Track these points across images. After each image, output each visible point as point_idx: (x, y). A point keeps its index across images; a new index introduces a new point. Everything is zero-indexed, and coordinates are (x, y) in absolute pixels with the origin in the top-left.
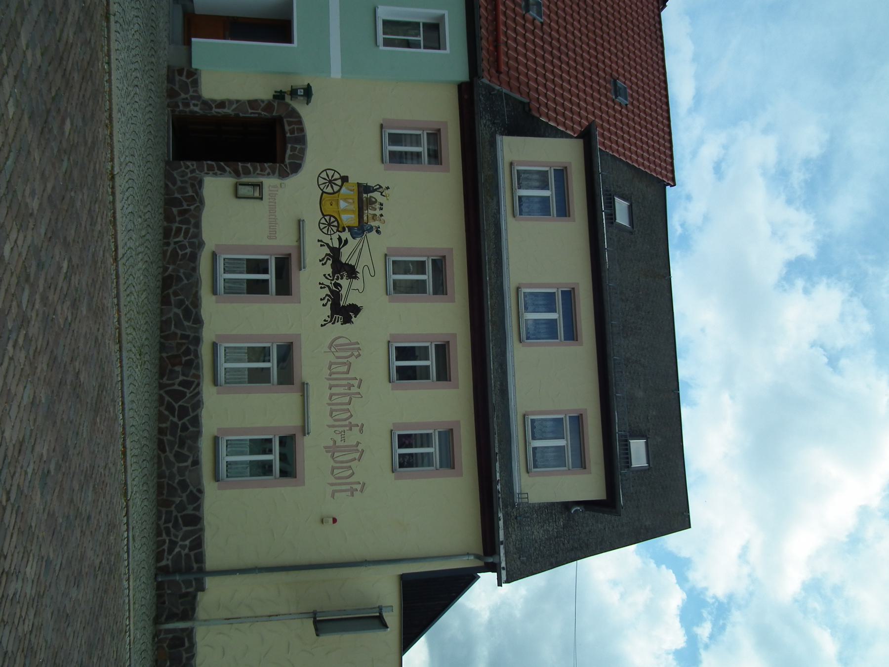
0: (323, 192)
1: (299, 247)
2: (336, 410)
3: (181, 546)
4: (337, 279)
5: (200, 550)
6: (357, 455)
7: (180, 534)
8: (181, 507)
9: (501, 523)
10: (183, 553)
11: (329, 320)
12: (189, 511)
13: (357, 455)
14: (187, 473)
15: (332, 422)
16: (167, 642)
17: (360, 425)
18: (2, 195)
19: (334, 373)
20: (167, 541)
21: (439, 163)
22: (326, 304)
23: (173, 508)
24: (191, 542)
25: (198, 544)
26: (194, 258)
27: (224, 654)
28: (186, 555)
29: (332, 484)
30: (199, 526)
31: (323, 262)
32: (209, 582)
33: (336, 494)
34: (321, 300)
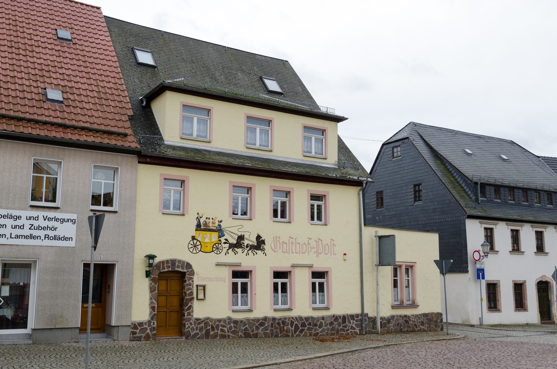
0: (201, 251)
1: (229, 265)
2: (302, 251)
3: (353, 324)
4: (244, 246)
8: (339, 325)
11: (263, 252)
12: (340, 321)
13: (320, 242)
14: (327, 322)
19: (287, 250)
23: (339, 328)
25: (352, 317)
28: (356, 322)
29: (331, 255)
30: (346, 316)
31: (236, 253)
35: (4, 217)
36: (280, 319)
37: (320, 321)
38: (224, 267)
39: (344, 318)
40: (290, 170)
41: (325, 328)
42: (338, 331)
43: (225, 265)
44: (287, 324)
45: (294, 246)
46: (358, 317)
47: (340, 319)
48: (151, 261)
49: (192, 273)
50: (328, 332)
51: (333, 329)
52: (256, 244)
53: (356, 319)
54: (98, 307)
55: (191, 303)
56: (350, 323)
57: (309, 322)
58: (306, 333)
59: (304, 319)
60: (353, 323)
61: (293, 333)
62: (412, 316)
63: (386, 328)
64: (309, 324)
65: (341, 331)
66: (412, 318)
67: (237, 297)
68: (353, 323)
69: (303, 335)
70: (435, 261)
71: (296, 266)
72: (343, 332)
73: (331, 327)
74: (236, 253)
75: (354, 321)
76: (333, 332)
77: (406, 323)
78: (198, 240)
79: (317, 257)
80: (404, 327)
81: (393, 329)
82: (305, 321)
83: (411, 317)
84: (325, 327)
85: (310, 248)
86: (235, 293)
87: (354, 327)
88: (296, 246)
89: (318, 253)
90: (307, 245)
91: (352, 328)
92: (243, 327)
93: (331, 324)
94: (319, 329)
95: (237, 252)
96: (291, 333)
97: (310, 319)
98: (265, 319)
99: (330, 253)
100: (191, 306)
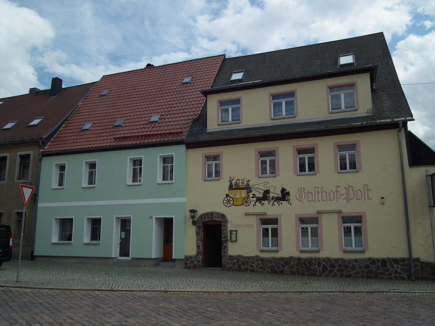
0: (233, 204)
6: (351, 189)
7: (391, 269)
9: (382, 121)
11: (288, 202)
13: (351, 189)
15: (335, 200)
17: (336, 187)
22: (281, 203)
24: (395, 264)
26: (263, 260)
29: (365, 199)
30: (387, 260)
31: (263, 204)
33: (370, 197)
48: (192, 214)
78: (230, 197)
99: (363, 198)
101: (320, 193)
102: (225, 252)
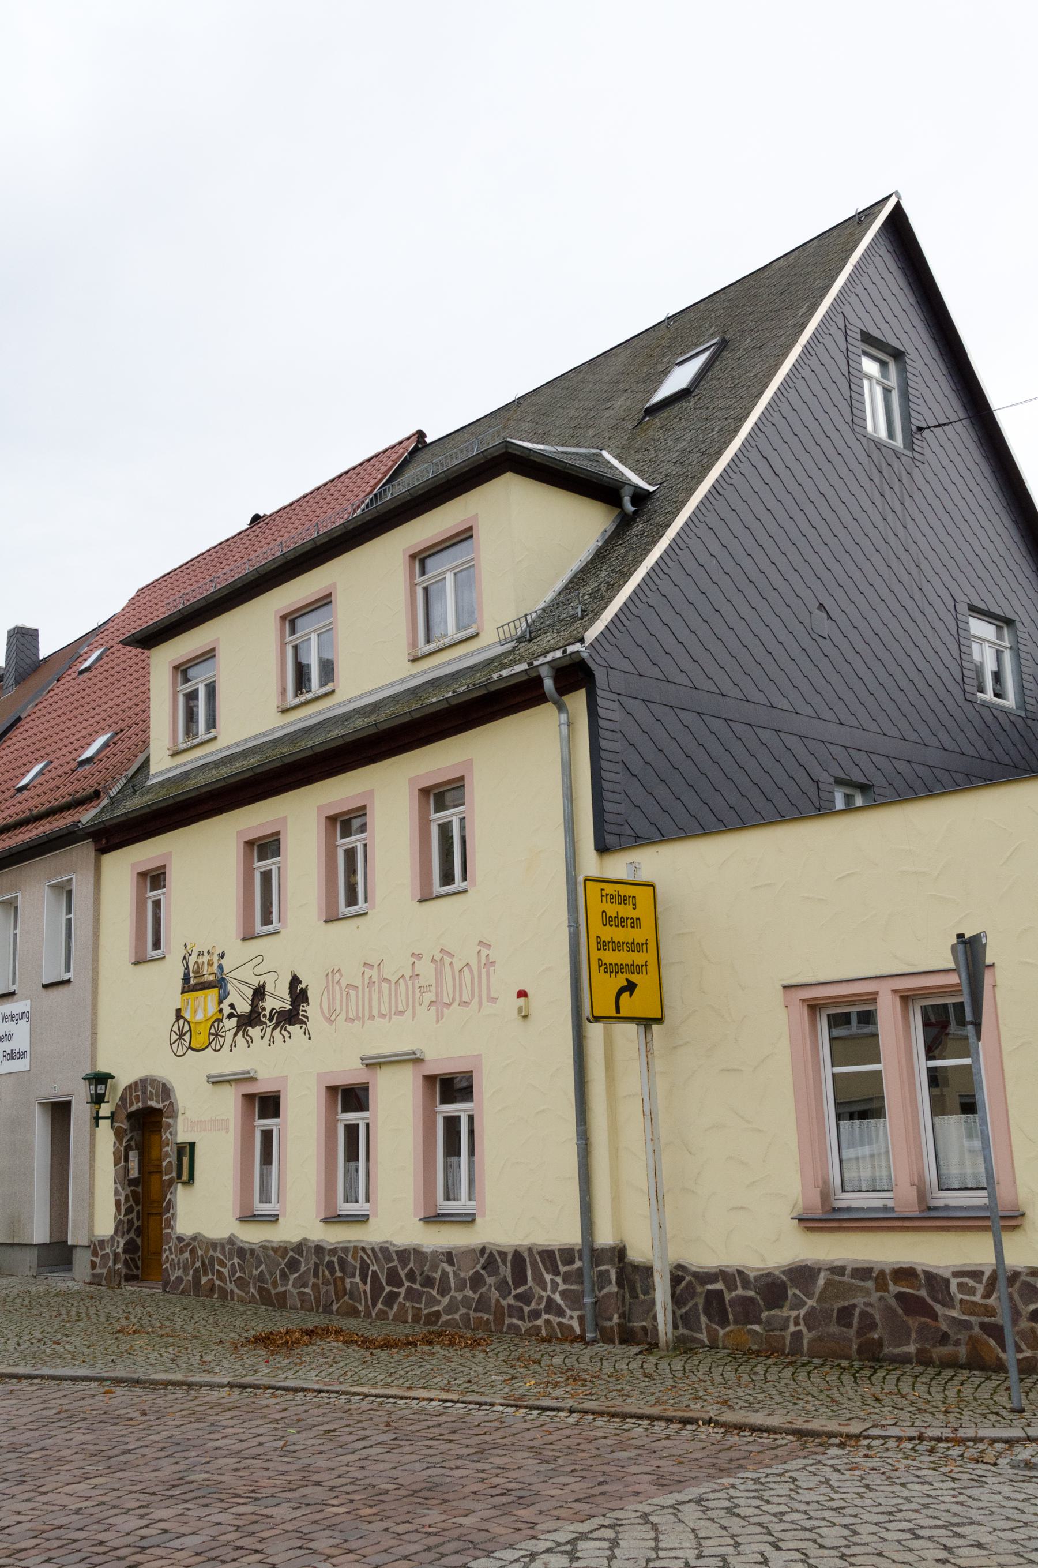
0: (190, 1048)
1: (237, 1081)
2: (397, 1007)
3: (554, 1292)
4: (265, 1016)
5: (557, 1253)
6: (447, 959)
7: (538, 1290)
8: (503, 1288)
9: (505, 673)
10: (562, 1287)
11: (304, 1026)
12: (506, 1271)
13: (447, 959)
14: (462, 1275)
15: (409, 1013)
16: (715, 1326)
17: (413, 960)
18: (847, 1564)
19: (357, 1014)
20: (547, 1316)
21: (163, 871)
22: (289, 1033)
23: (504, 1303)
24: (548, 1273)
25: (548, 1256)
26: (243, 1252)
27: (744, 1208)
28: (564, 1282)
29: (480, 1003)
30: (526, 1255)
31: (250, 1041)
32: (605, 1237)
33: (493, 995)
34: (285, 1042)
35: (6, 1018)
36: (333, 1251)
37: (440, 1269)
38: (227, 1085)
39: (518, 1259)
40: (434, 700)
41: (459, 1296)
42: (499, 1314)
43: (228, 1081)
44: (349, 1270)
45: (377, 990)
46: (571, 1262)
47: (504, 1263)
48: (101, 1089)
49: (174, 1115)
50: (468, 1314)
51: (482, 1305)
52: (289, 1007)
53: (563, 1269)
54: (693, 1192)
55: (171, 1193)
56: (543, 1285)
57: (409, 1267)
58: (402, 1306)
59: (395, 1256)
60: (555, 1285)
61: (370, 1303)
62: (957, 1274)
63: (756, 1327)
64: (411, 1276)
65: (510, 1316)
66: (960, 1286)
67: (357, 1170)
68: (555, 1285)
69: (395, 1315)
70: (631, 995)
71: (380, 1064)
72: (520, 1323)
73: (476, 1297)
74: (250, 1041)
75: (559, 1279)
76: (485, 1316)
77: (908, 1312)
78: (185, 1020)
79: (437, 1022)
80: (901, 1334)
81: (807, 1336)
82: (396, 1263)
83: (954, 1282)
84: (457, 1294)
85: (417, 990)
86: (454, 1155)
87: (558, 1305)
88: (380, 991)
89: (440, 1005)
90: (410, 983)
91: (551, 1306)
92: (257, 1270)
93: (476, 1281)
94: (438, 1297)
95: (289, 1033)
96: (363, 1302)
97: (412, 1257)
98: (300, 1247)
99: (476, 999)
100: (170, 1201)
101: (377, 984)
102: (169, 1226)
